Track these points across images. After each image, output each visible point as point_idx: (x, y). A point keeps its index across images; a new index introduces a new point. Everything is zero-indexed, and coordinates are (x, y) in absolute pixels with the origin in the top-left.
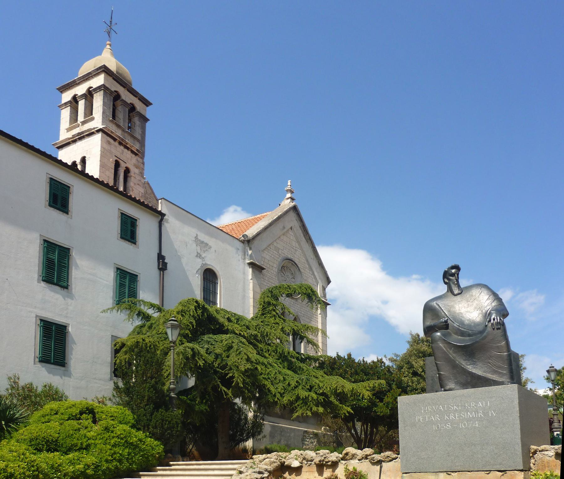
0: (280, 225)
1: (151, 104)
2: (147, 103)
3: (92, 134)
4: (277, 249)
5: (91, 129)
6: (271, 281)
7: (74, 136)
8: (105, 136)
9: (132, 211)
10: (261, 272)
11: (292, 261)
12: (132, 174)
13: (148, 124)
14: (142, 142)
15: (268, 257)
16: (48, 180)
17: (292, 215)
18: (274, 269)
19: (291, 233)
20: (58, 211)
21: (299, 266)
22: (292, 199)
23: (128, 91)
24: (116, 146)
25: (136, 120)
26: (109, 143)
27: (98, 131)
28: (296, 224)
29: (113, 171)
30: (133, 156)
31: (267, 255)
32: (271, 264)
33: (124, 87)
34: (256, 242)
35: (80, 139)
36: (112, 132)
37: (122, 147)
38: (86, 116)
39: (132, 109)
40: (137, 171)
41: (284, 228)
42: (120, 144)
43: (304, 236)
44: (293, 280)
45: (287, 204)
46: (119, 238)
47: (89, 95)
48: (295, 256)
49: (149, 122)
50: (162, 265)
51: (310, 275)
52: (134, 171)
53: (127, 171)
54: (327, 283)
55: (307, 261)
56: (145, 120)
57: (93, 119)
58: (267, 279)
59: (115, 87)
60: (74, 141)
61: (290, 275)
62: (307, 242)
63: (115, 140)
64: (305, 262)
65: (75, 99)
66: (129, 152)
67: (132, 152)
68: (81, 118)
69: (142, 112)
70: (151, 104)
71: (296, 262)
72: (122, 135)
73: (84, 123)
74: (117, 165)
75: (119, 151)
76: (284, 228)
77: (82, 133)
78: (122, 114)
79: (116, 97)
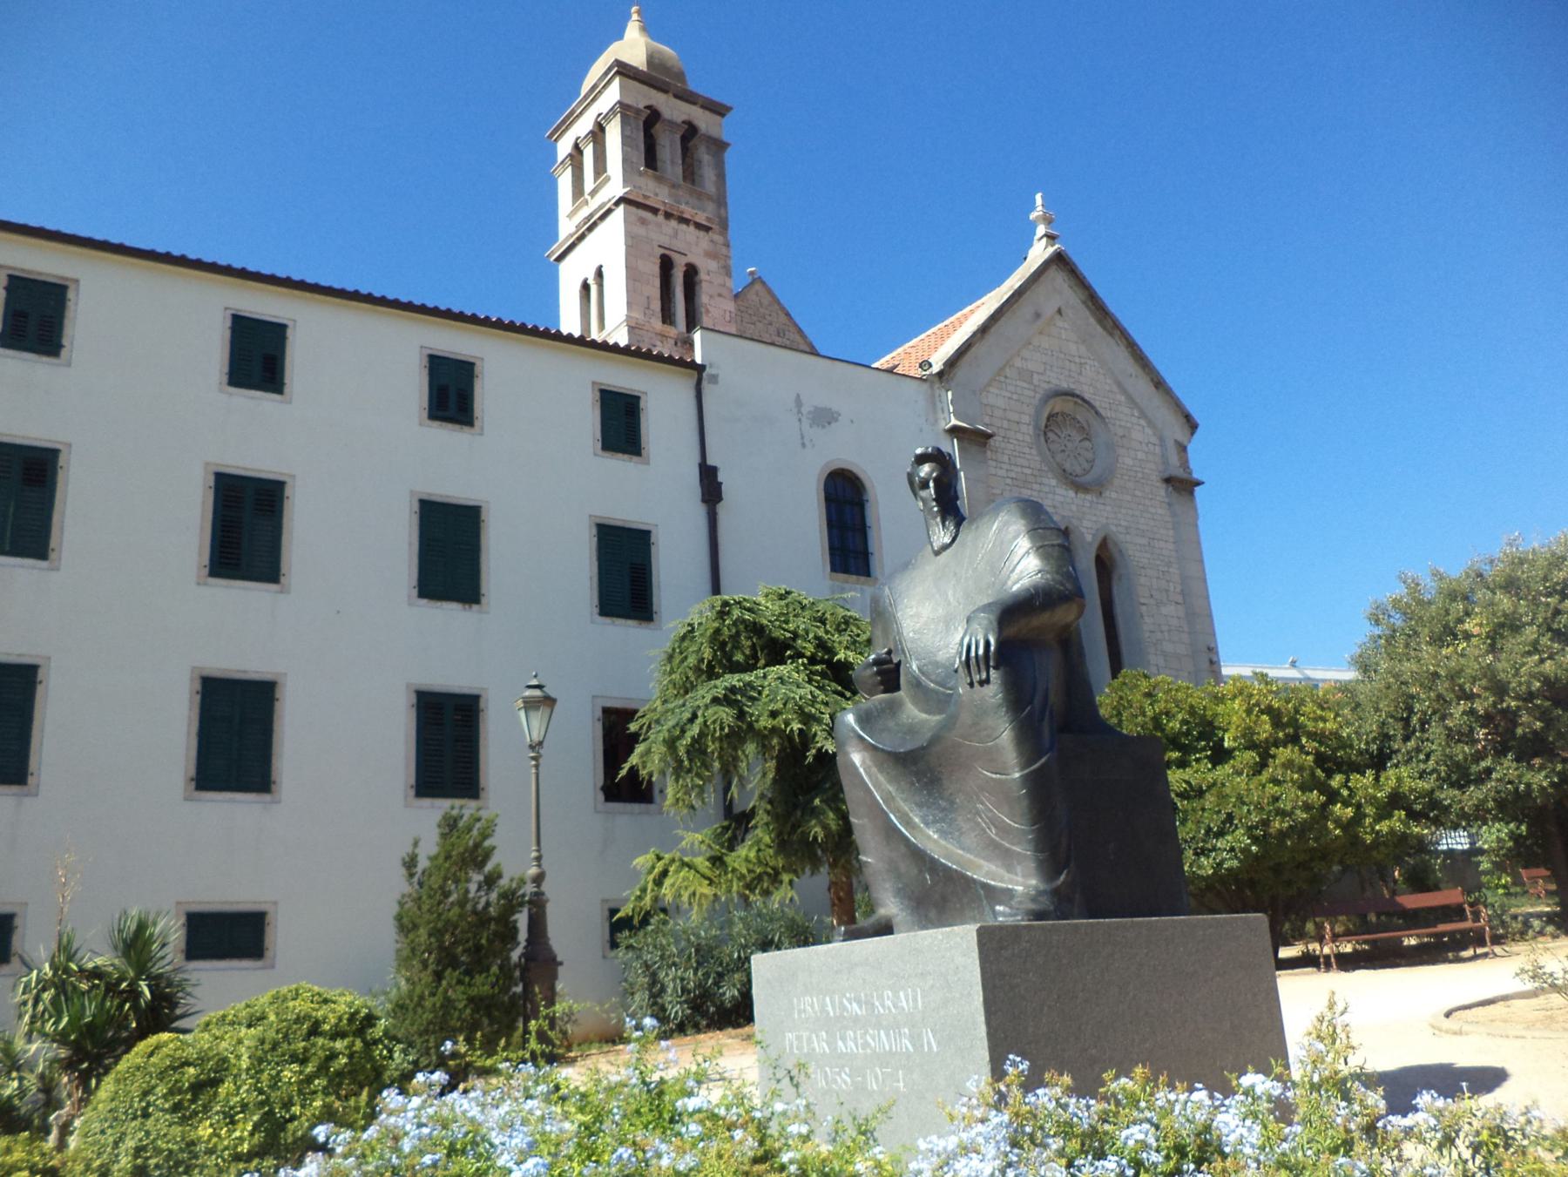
0: (1025, 309)
1: (729, 109)
2: (719, 110)
3: (609, 211)
4: (1026, 375)
5: (604, 205)
6: (1020, 461)
7: (578, 227)
8: (633, 209)
9: (625, 378)
10: (985, 445)
11: (1073, 395)
12: (703, 276)
13: (729, 156)
14: (721, 201)
15: (1001, 403)
16: (425, 362)
17: (1058, 277)
18: (1024, 428)
19: (1060, 324)
20: (450, 426)
21: (1097, 404)
22: (1051, 238)
23: (676, 96)
24: (659, 225)
25: (704, 156)
26: (643, 222)
27: (617, 204)
28: (1067, 295)
29: (657, 282)
30: (702, 234)
31: (996, 398)
32: (1015, 417)
33: (665, 91)
34: (961, 372)
35: (590, 229)
36: (645, 197)
37: (673, 223)
38: (596, 178)
39: (690, 132)
40: (713, 265)
41: (1038, 315)
42: (668, 216)
43: (1100, 322)
44: (1087, 443)
45: (1039, 252)
46: (599, 451)
47: (598, 133)
48: (1082, 379)
49: (729, 150)
50: (711, 487)
51: (1134, 420)
52: (708, 269)
53: (691, 272)
54: (1187, 431)
55: (1119, 384)
56: (719, 146)
57: (608, 179)
58: (1006, 458)
59: (646, 97)
60: (582, 238)
61: (1074, 433)
62: (1111, 334)
63: (655, 211)
64: (1115, 389)
65: (578, 150)
66: (692, 228)
67: (699, 226)
68: (589, 184)
69: (714, 132)
70: (729, 109)
71: (1087, 396)
72: (670, 195)
73: (593, 193)
74: (666, 264)
75: (665, 234)
76: (1038, 315)
77: (591, 215)
78: (669, 148)
79: (652, 118)
